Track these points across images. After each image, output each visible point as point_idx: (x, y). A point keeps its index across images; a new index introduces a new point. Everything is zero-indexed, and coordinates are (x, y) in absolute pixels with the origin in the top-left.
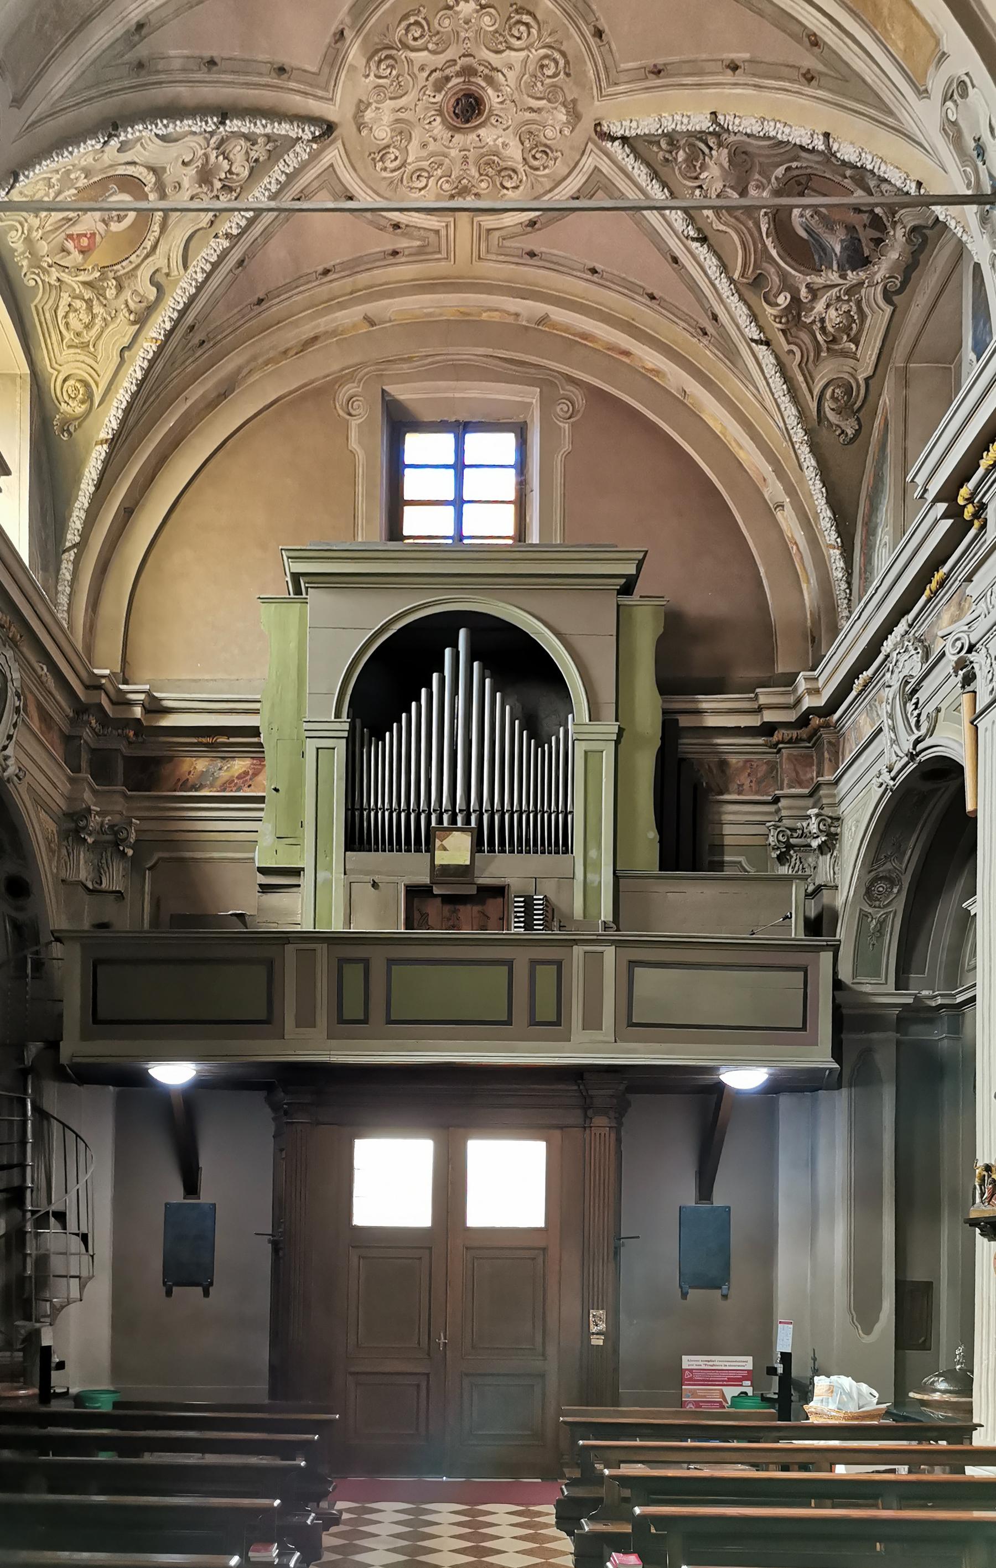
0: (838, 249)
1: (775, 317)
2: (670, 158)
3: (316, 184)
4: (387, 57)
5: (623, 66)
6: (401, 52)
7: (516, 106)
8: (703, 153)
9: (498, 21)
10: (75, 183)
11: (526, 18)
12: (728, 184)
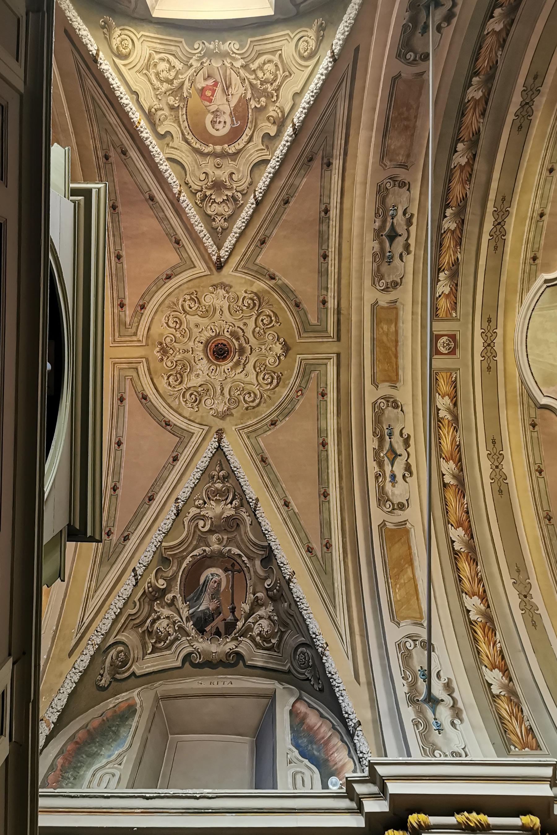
0: (202, 608)
1: (150, 582)
2: (215, 479)
3: (185, 255)
4: (255, 304)
5: (260, 439)
6: (256, 312)
7: (223, 380)
8: (227, 499)
9: (271, 366)
10: (254, 99)
11: (275, 382)
12: (213, 520)
